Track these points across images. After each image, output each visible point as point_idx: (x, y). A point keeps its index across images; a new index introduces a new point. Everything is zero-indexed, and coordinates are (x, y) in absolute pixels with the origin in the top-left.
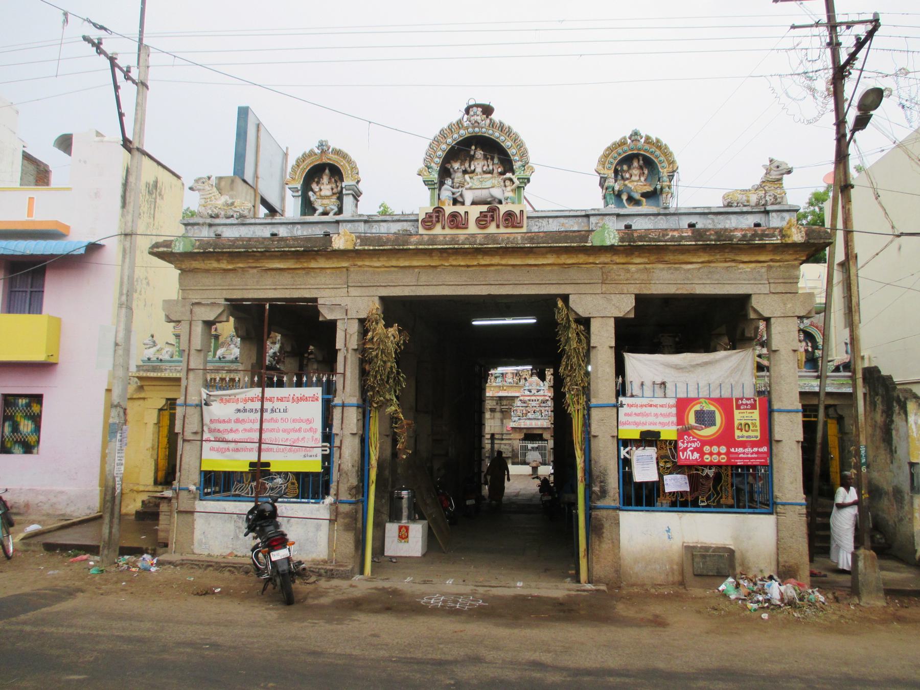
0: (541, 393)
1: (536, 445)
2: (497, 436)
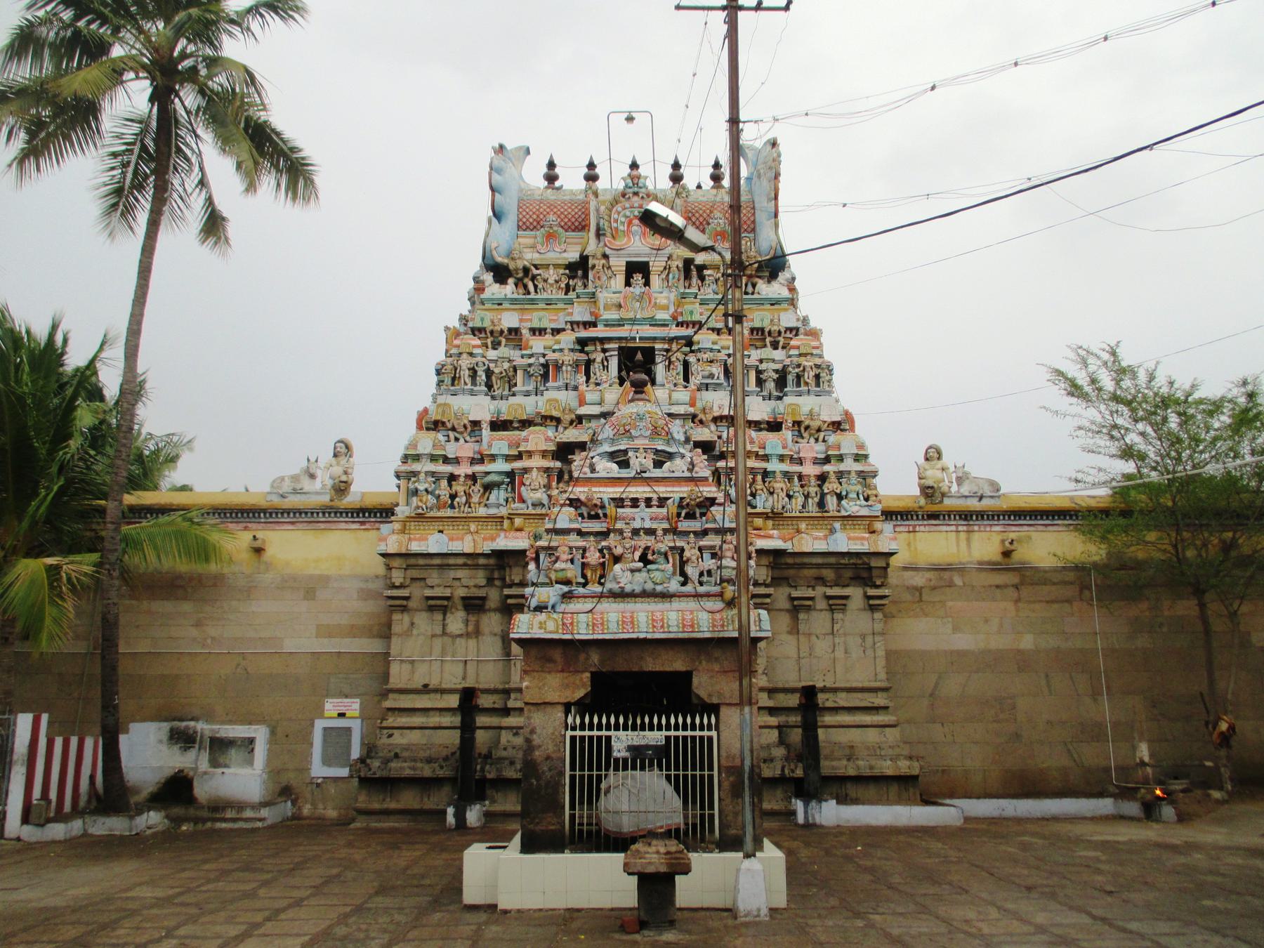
0: (678, 467)
1: (655, 737)
2: (485, 701)
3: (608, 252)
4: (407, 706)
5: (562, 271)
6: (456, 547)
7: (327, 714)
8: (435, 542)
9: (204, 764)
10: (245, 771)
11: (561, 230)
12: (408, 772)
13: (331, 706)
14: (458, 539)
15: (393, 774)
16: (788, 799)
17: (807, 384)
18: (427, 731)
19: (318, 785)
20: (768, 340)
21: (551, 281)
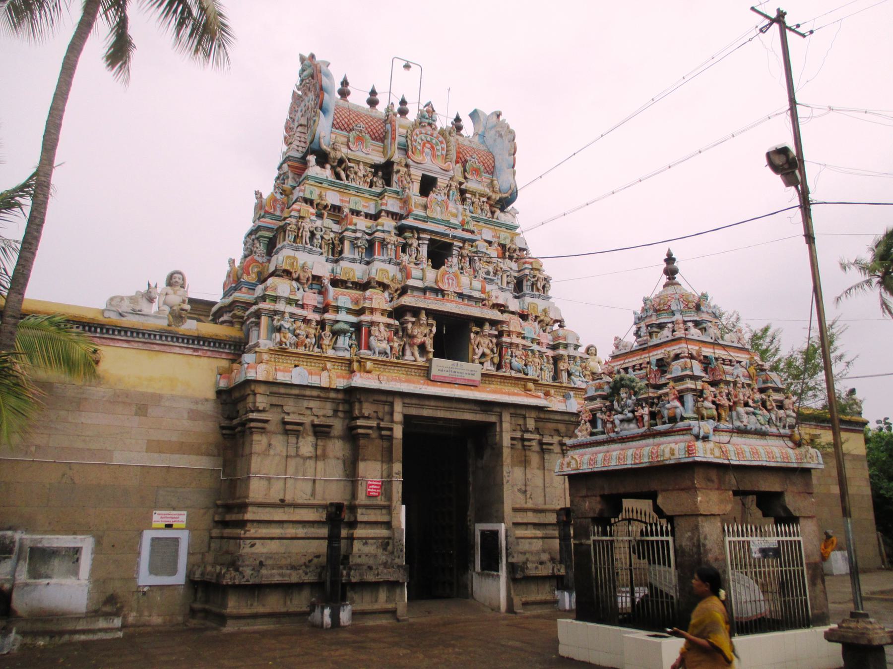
3: (411, 163)
4: (266, 519)
5: (369, 169)
6: (314, 381)
7: (154, 525)
8: (299, 375)
9: (22, 576)
10: (70, 581)
11: (367, 136)
12: (277, 579)
13: (159, 518)
14: (316, 374)
15: (265, 581)
16: (553, 592)
17: (538, 290)
18: (285, 541)
19: (144, 593)
20: (507, 254)
21: (360, 174)
